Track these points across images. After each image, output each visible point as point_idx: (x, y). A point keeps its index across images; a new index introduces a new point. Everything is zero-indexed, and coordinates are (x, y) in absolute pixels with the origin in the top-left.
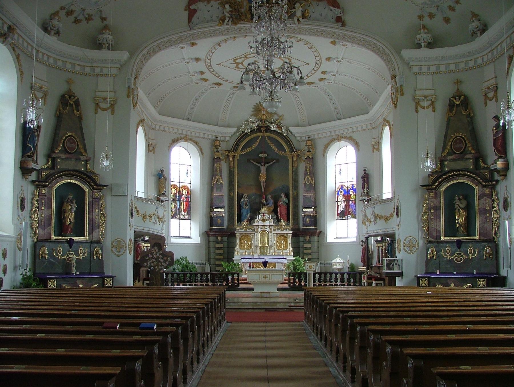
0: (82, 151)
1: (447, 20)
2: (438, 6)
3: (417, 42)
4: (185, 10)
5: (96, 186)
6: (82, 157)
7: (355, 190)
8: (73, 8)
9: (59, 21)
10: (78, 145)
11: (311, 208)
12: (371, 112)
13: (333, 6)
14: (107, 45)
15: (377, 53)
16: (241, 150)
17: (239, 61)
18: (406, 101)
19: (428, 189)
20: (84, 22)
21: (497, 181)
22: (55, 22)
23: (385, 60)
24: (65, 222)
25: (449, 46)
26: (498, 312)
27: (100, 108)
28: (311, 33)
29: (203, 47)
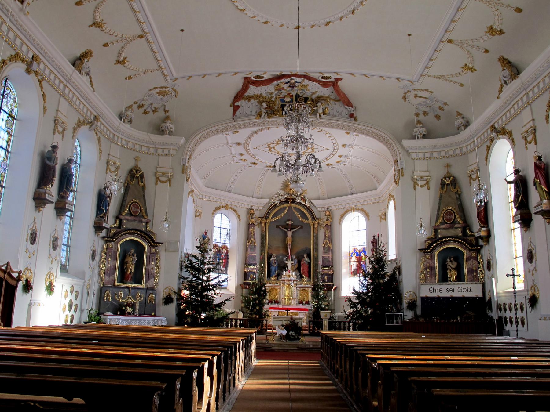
0: (144, 214)
1: (438, 117)
2: (430, 107)
3: (414, 134)
4: (231, 106)
5: (153, 243)
6: (143, 220)
7: (365, 253)
8: (143, 102)
9: (132, 112)
10: (141, 210)
11: (329, 267)
12: (378, 189)
13: (348, 106)
14: (168, 131)
15: (383, 142)
16: (272, 218)
17: (272, 146)
18: (406, 180)
19: (424, 253)
20: (151, 113)
21: (482, 247)
22: (129, 113)
23: (389, 148)
24: (127, 271)
25: (440, 138)
26: (474, 350)
27: (160, 181)
28: (330, 126)
29: (244, 133)
